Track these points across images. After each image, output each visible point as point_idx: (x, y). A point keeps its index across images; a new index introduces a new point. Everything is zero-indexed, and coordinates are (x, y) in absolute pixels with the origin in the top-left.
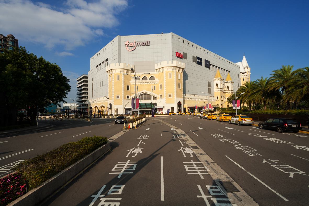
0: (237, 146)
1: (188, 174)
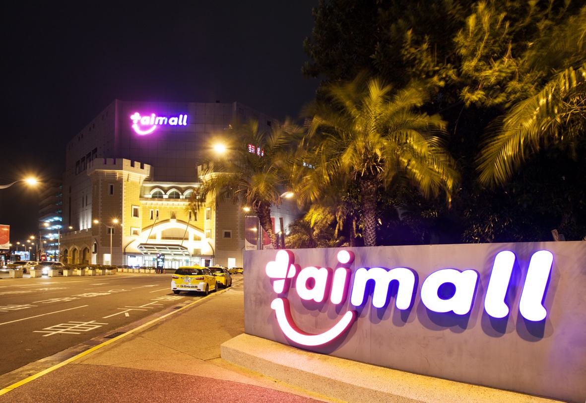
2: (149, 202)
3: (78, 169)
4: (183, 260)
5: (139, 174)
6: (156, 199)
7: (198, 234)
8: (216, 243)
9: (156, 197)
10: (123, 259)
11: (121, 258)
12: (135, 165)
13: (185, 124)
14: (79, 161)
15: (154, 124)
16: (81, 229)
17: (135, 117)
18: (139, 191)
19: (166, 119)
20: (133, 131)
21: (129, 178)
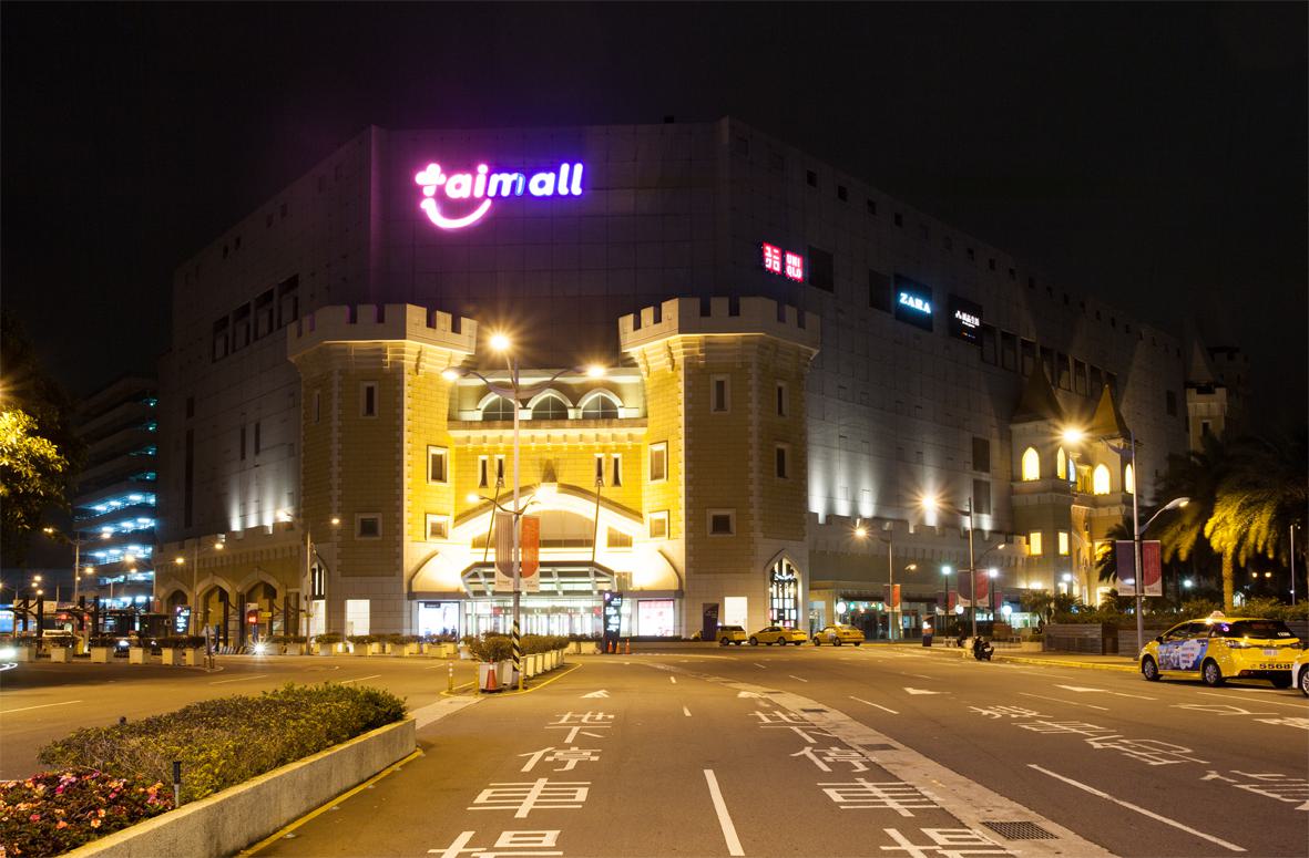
0: (1096, 741)
1: (842, 807)
2: (476, 434)
3: (220, 343)
4: (582, 611)
5: (448, 350)
6: (499, 423)
7: (623, 525)
8: (689, 553)
9: (496, 418)
10: (406, 615)
11: (400, 612)
12: (359, 318)
13: (577, 190)
14: (225, 319)
15: (486, 196)
16: (236, 526)
17: (430, 177)
18: (446, 401)
19: (521, 180)
20: (422, 218)
21: (421, 364)
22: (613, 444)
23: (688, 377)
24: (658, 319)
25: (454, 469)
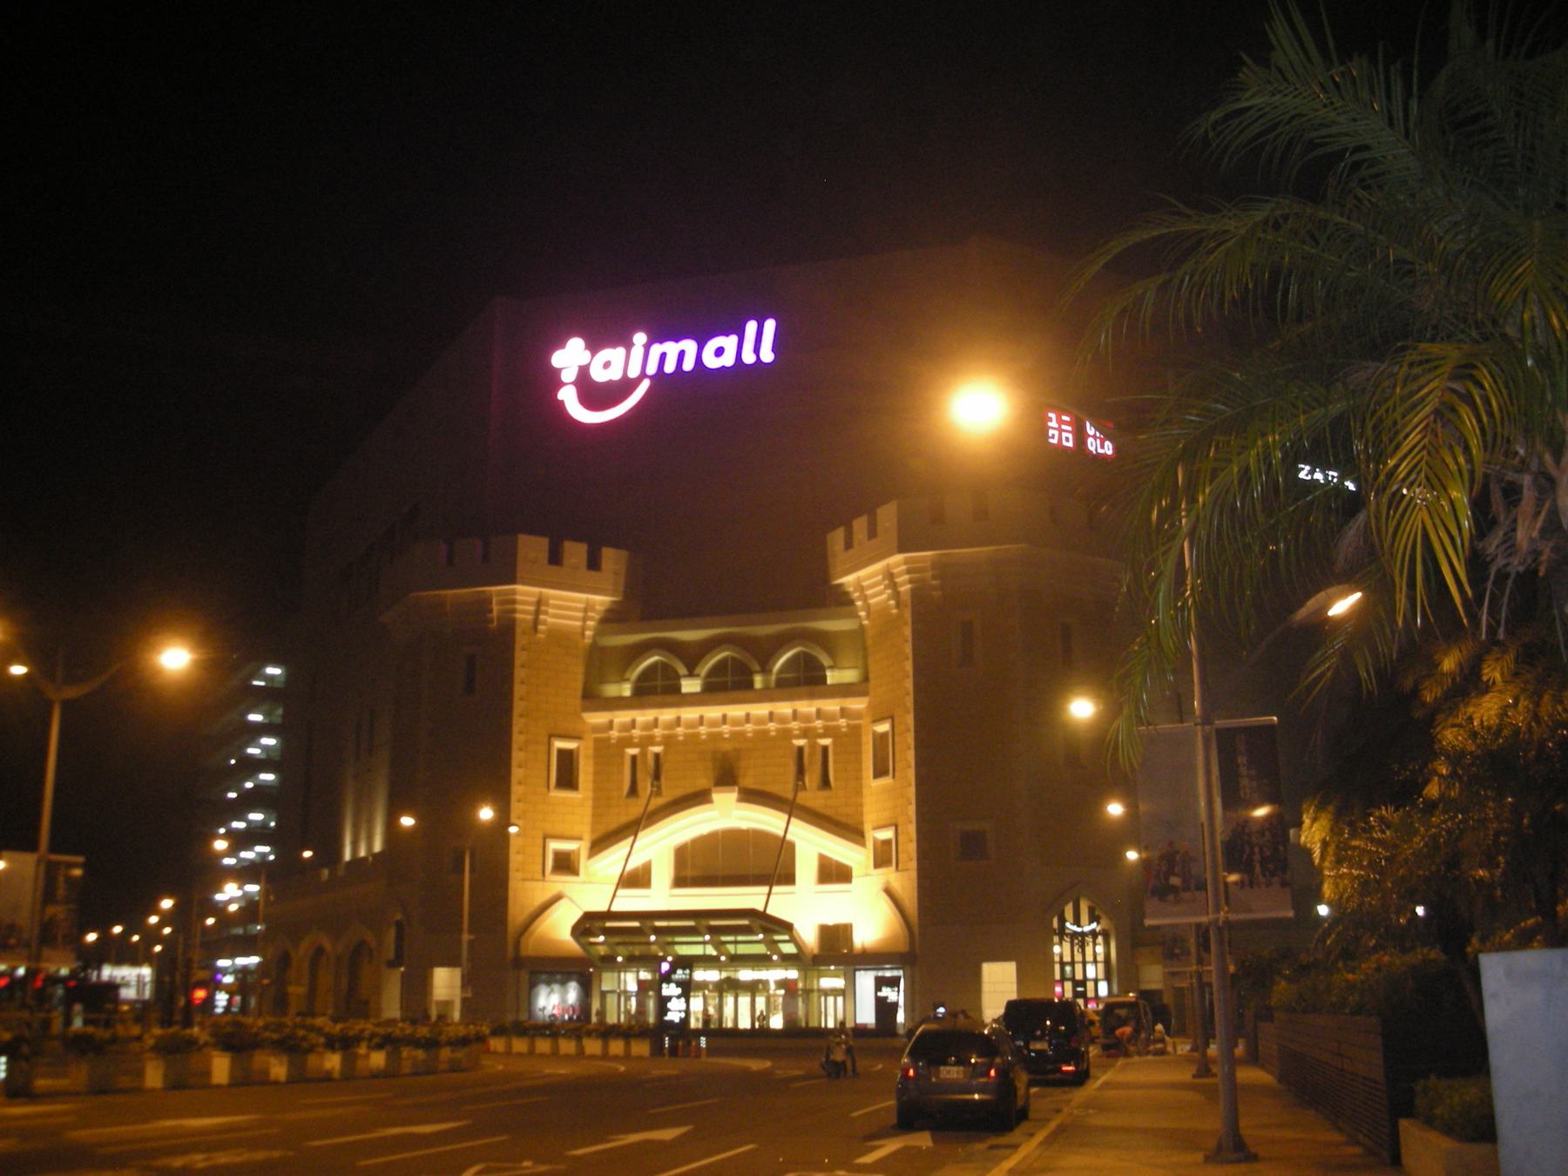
13: (767, 356)
15: (643, 375)
17: (570, 357)
22: (819, 723)
23: (915, 613)
24: (872, 533)
25: (591, 769)
